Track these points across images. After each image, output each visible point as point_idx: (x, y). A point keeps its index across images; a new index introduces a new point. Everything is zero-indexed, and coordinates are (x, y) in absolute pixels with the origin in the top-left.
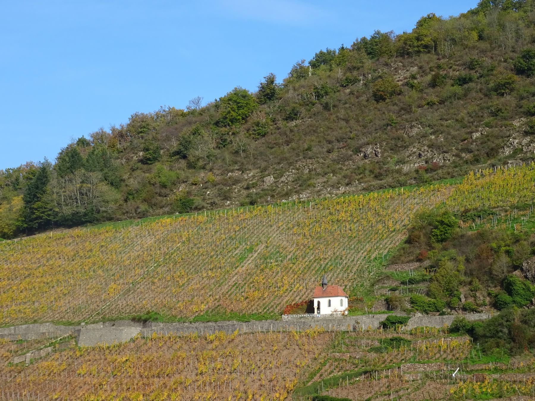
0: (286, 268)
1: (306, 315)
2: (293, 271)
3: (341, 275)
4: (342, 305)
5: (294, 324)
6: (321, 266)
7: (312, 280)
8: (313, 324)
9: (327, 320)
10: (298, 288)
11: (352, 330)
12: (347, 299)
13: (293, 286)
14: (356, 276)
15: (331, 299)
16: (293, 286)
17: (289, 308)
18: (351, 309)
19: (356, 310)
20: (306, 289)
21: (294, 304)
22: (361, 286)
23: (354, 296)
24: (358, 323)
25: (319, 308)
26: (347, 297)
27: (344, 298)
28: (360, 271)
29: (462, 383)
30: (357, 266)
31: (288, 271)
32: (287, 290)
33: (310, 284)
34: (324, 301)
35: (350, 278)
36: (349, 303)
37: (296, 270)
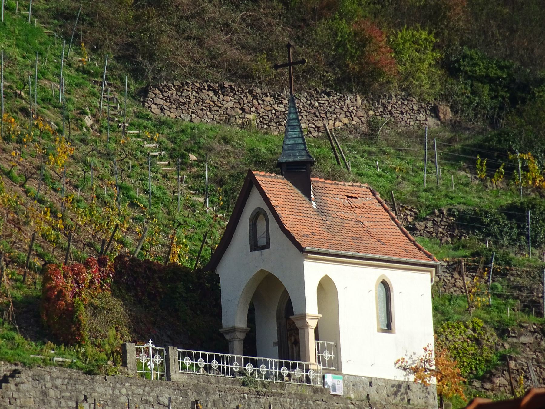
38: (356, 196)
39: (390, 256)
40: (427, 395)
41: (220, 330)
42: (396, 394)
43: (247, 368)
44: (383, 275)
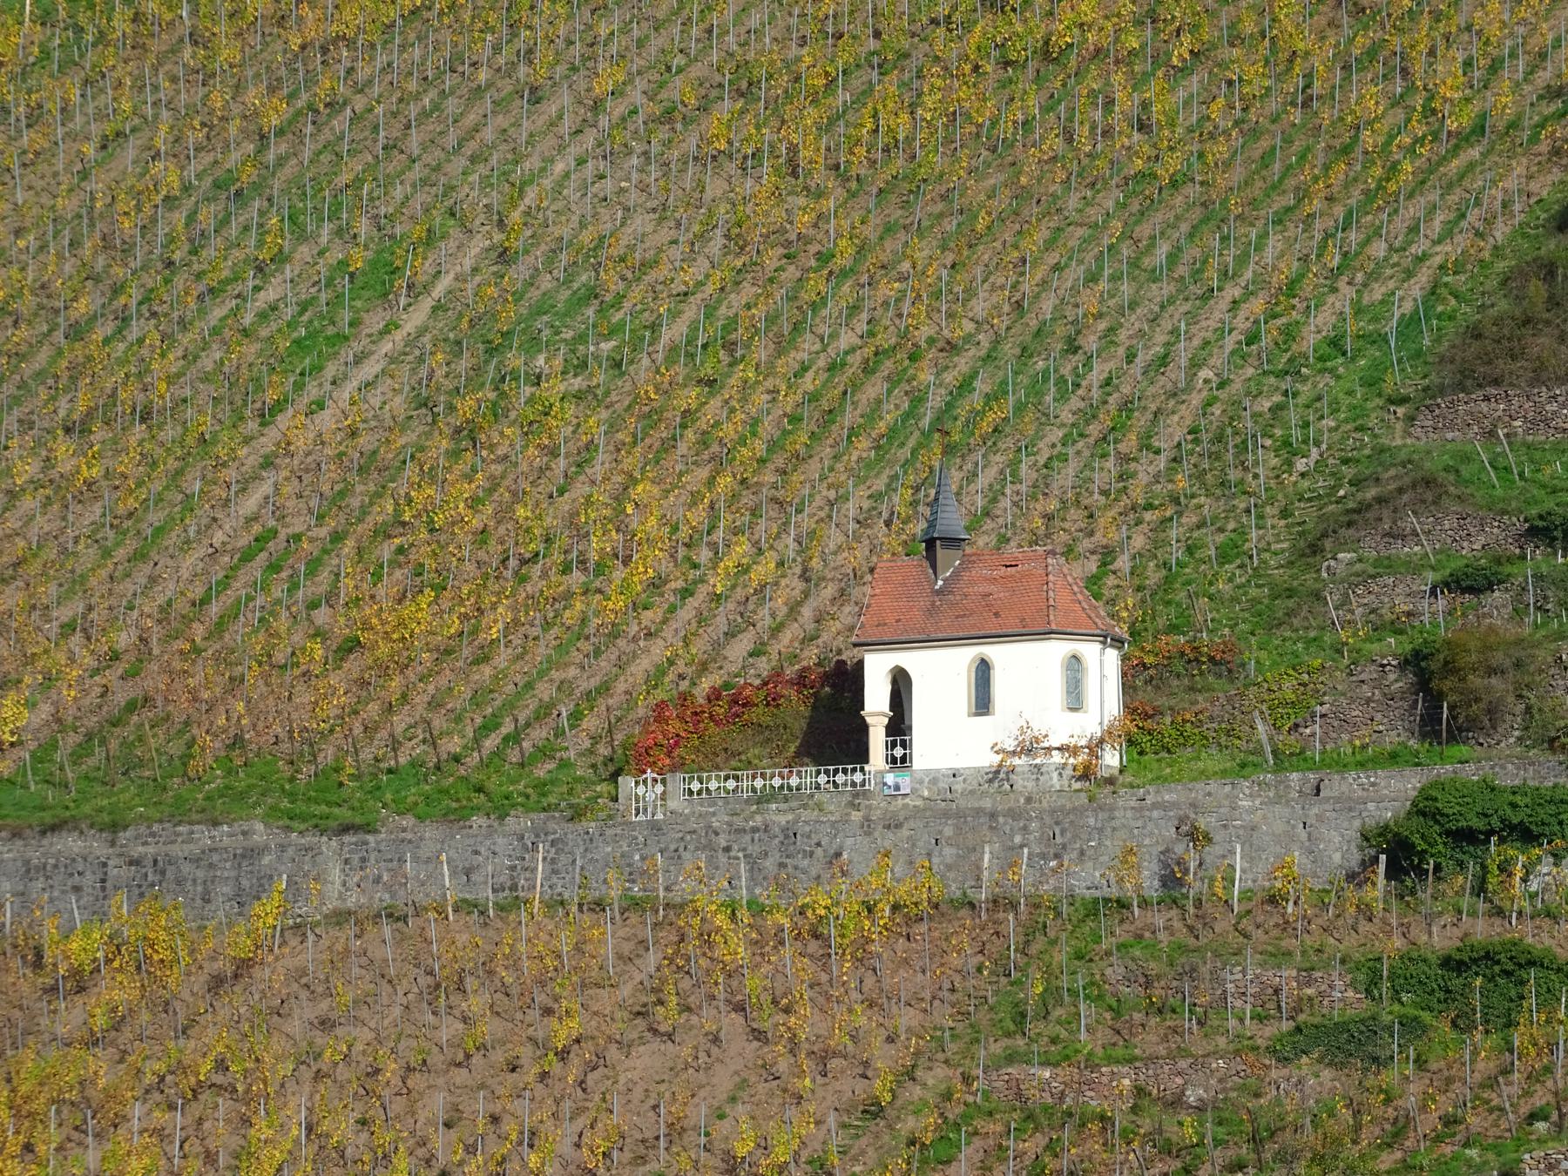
1: (806, 777)
4: (1075, 700)
5: (710, 847)
6: (917, 399)
7: (851, 508)
8: (854, 848)
9: (960, 815)
10: (744, 570)
11: (1150, 885)
12: (1112, 656)
13: (704, 555)
14: (1182, 483)
15: (996, 653)
16: (704, 555)
17: (674, 727)
18: (1147, 726)
19: (1184, 740)
20: (805, 576)
21: (715, 695)
22: (1224, 557)
23: (1173, 629)
24: (1197, 837)
25: (899, 726)
26: (1118, 642)
27: (1090, 651)
28: (1220, 438)
30: (1196, 400)
31: (669, 444)
32: (656, 585)
33: (834, 538)
34: (938, 673)
37: (729, 431)
42: (990, 781)
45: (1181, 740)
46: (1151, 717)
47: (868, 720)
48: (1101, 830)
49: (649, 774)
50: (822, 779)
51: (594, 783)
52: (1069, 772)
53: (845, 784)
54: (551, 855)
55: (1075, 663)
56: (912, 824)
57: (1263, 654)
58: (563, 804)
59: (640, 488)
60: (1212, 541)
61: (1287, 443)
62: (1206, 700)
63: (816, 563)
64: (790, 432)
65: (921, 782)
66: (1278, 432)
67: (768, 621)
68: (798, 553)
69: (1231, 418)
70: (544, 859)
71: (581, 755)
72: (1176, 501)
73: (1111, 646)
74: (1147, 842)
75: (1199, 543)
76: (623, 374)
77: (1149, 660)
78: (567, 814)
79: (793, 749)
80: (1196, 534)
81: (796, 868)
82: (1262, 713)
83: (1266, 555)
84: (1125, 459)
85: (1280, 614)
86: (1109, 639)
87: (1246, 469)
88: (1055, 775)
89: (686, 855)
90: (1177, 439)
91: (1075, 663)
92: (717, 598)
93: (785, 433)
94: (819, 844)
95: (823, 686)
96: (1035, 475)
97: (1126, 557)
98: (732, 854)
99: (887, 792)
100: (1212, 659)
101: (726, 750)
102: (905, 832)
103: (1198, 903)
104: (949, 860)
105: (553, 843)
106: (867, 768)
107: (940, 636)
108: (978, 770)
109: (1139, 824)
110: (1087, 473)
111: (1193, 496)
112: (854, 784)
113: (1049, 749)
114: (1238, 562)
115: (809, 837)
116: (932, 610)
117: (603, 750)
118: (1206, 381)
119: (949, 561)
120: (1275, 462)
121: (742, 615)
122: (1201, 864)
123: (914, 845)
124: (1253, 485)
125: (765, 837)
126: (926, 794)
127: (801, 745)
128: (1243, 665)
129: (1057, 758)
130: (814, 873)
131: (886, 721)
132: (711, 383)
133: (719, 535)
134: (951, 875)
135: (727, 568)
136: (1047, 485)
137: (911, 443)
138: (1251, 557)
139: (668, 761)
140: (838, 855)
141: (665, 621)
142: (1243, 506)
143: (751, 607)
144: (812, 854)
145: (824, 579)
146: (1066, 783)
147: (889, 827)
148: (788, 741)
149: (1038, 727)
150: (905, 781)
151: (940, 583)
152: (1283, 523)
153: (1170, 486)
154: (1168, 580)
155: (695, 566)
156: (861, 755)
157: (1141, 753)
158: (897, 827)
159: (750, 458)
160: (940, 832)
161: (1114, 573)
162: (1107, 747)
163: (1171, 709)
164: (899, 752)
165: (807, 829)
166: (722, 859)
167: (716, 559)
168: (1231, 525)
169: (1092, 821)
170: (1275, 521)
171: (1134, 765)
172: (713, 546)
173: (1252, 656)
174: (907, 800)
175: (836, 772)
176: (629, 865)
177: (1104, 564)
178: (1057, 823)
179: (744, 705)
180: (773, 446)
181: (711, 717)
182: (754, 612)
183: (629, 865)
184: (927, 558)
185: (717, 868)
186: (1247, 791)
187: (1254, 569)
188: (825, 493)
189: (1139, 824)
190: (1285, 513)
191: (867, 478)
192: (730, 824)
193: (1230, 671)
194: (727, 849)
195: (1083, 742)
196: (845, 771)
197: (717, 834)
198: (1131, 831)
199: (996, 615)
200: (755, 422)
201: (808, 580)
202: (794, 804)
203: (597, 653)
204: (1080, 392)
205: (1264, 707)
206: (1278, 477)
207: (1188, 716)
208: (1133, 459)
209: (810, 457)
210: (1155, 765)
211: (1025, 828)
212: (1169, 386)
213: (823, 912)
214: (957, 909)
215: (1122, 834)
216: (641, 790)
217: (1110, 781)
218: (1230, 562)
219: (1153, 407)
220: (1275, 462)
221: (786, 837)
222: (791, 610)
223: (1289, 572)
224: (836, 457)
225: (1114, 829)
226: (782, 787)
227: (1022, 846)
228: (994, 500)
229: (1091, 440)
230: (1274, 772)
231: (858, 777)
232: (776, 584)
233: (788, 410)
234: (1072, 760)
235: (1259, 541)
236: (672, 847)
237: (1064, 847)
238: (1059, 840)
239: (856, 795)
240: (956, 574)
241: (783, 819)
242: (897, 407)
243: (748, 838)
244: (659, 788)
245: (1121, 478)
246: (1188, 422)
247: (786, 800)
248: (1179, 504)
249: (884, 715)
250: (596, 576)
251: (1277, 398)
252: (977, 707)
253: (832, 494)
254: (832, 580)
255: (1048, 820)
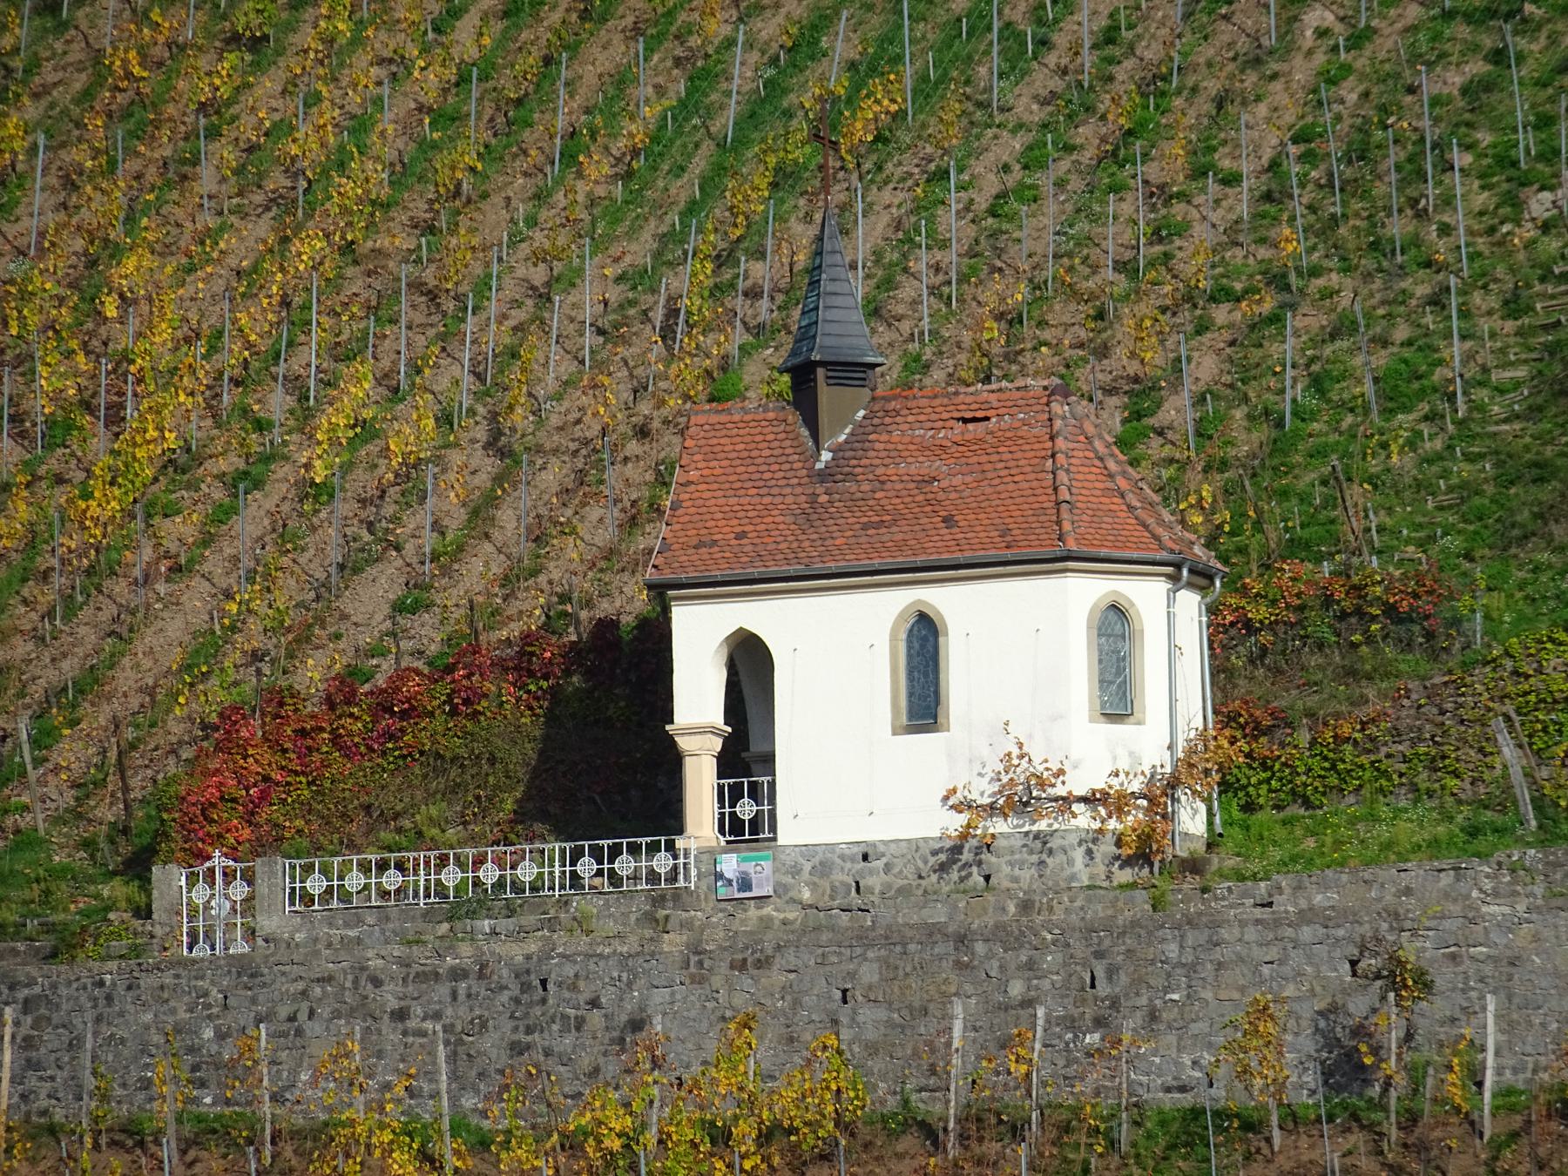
0: (139, 116)
1: (537, 864)
2: (247, 174)
3: (1052, 211)
4: (1117, 698)
5: (363, 1010)
6: (704, 74)
7: (587, 299)
8: (670, 1011)
9: (893, 938)
10: (365, 431)
11: (1304, 1086)
12: (1190, 603)
13: (277, 403)
14: (1292, 244)
15: (950, 601)
16: (277, 403)
17: (260, 760)
18: (1262, 746)
19: (1339, 780)
20: (495, 444)
21: (342, 691)
22: (1393, 397)
23: (1296, 547)
24: (1403, 980)
25: (746, 757)
26: (1201, 578)
27: (1147, 595)
28: (1361, 152)
29: (204, 669)
30: (1302, 72)
31: (181, 172)
32: (180, 465)
33: (551, 364)
34: (828, 647)
35: (1194, 258)
36: (1220, 673)
37: (306, 145)
38: (988, 414)
39: (982, 553)
40: (1044, 856)
41: (744, 755)
42: (943, 868)
43: (393, 888)
44: (919, 601)
45: (1333, 780)
46: (1268, 732)
47: (683, 743)
48: (1191, 968)
49: (218, 860)
50: (586, 866)
51: (92, 880)
52: (1107, 848)
53: (635, 878)
54: (24, 1030)
55: (1115, 623)
56: (791, 958)
57: (1496, 600)
58: (32, 925)
59: (131, 263)
60: (1366, 365)
61: (1505, 161)
62: (1383, 695)
63: (520, 418)
64: (435, 146)
65: (795, 871)
66: (1485, 138)
67: (429, 541)
68: (478, 396)
69: (1384, 110)
70: (13, 1037)
71: (57, 820)
72: (1278, 281)
73: (1190, 585)
74: (1290, 991)
75: (1336, 370)
76: (61, 27)
77: (1259, 613)
78: (45, 943)
79: (509, 805)
80: (1328, 351)
81: (548, 1053)
82: (1508, 718)
83: (1482, 394)
84: (1160, 194)
85: (1524, 516)
86: (1182, 571)
87: (1421, 215)
88: (1079, 855)
89: (314, 1028)
90: (1267, 155)
91: (1115, 623)
92: (314, 493)
93: (427, 148)
94: (594, 1003)
95: (568, 673)
96: (972, 231)
97: (1185, 399)
98: (412, 1024)
99: (723, 892)
100: (1390, 610)
101: (368, 808)
102: (776, 977)
103: (1411, 1119)
104: (871, 1035)
105: (27, 1006)
106: (680, 843)
107: (832, 566)
108: (915, 845)
109: (1273, 953)
110: (1083, 226)
111: (1315, 272)
112: (653, 877)
113: (1067, 801)
114: (1425, 407)
115: (574, 988)
116: (811, 513)
117: (107, 812)
118: (1322, 33)
119: (844, 412)
120: (1482, 199)
121: (370, 527)
122: (1409, 1036)
123: (797, 1003)
124: (1442, 250)
125: (480, 988)
126: (806, 895)
127: (527, 797)
128: (1456, 622)
129: (1083, 819)
130: (586, 1062)
131: (718, 744)
132: (257, 43)
133: (309, 357)
134: (876, 1065)
135: (333, 428)
136: (999, 252)
137: (699, 164)
138: (1452, 397)
139: (246, 833)
140: (637, 1025)
141: (207, 540)
142: (1422, 290)
143: (389, 509)
144: (580, 1023)
145: (539, 449)
146: (1101, 869)
147: (742, 966)
148: (497, 787)
149: (1042, 756)
150: (762, 870)
151: (826, 456)
152: (1510, 325)
153: (1264, 253)
154: (1279, 446)
155: (261, 426)
156: (667, 817)
157: (1249, 807)
158: (759, 964)
159: (359, 201)
160: (852, 975)
161: (1160, 433)
162: (1183, 795)
163: (1310, 714)
164: (746, 809)
165: (569, 970)
166: (390, 1035)
167: (304, 416)
168: (1402, 332)
169: (1172, 950)
170: (1496, 322)
171: (1236, 832)
172: (296, 385)
173: (1479, 608)
174: (768, 910)
175: (615, 852)
176: (191, 1050)
177: (1138, 415)
178: (1099, 955)
179: (404, 715)
180: (402, 173)
181: (336, 739)
182: (395, 519)
183: (191, 1050)
184: (797, 404)
185: (380, 1054)
186: (1488, 885)
187: (1460, 423)
188: (521, 272)
189: (1273, 953)
190: (1514, 306)
191: (611, 238)
192: (405, 963)
193: (1430, 635)
194: (400, 1015)
195: (1136, 786)
196: (634, 850)
197: (377, 982)
198: (1256, 971)
199: (948, 521)
200: (359, 126)
201: (503, 453)
202: (530, 920)
203: (70, 607)
204: (1052, 59)
205: (1509, 708)
206: (1492, 230)
207: (1346, 730)
208: (1181, 196)
209: (485, 196)
210: (1280, 833)
211: (1030, 965)
212: (1243, 44)
213: (616, 1144)
214: (893, 1135)
215: (1239, 975)
216: (200, 894)
217: (1193, 866)
218: (1406, 409)
219: (1213, 86)
220: (1482, 199)
221: (526, 988)
222: (475, 513)
223: (1533, 429)
224: (540, 197)
225: (1220, 966)
226: (500, 885)
227: (1028, 1003)
228: (888, 284)
229: (1087, 156)
230: (1542, 844)
231: (662, 862)
232: (437, 460)
233: (431, 98)
234: (1113, 824)
235: (1464, 363)
236: (284, 1011)
237: (1115, 1004)
238: (1103, 989)
239: (659, 900)
240: (860, 438)
241: (516, 952)
242: (660, 91)
243: (443, 990)
244: (239, 890)
245: (1157, 236)
246: (1289, 117)
247: (511, 912)
248: (1288, 288)
249: (714, 731)
250: (49, 447)
251: (1477, 67)
252: (912, 714)
253: (539, 275)
254: (555, 451)
255: (1079, 949)
